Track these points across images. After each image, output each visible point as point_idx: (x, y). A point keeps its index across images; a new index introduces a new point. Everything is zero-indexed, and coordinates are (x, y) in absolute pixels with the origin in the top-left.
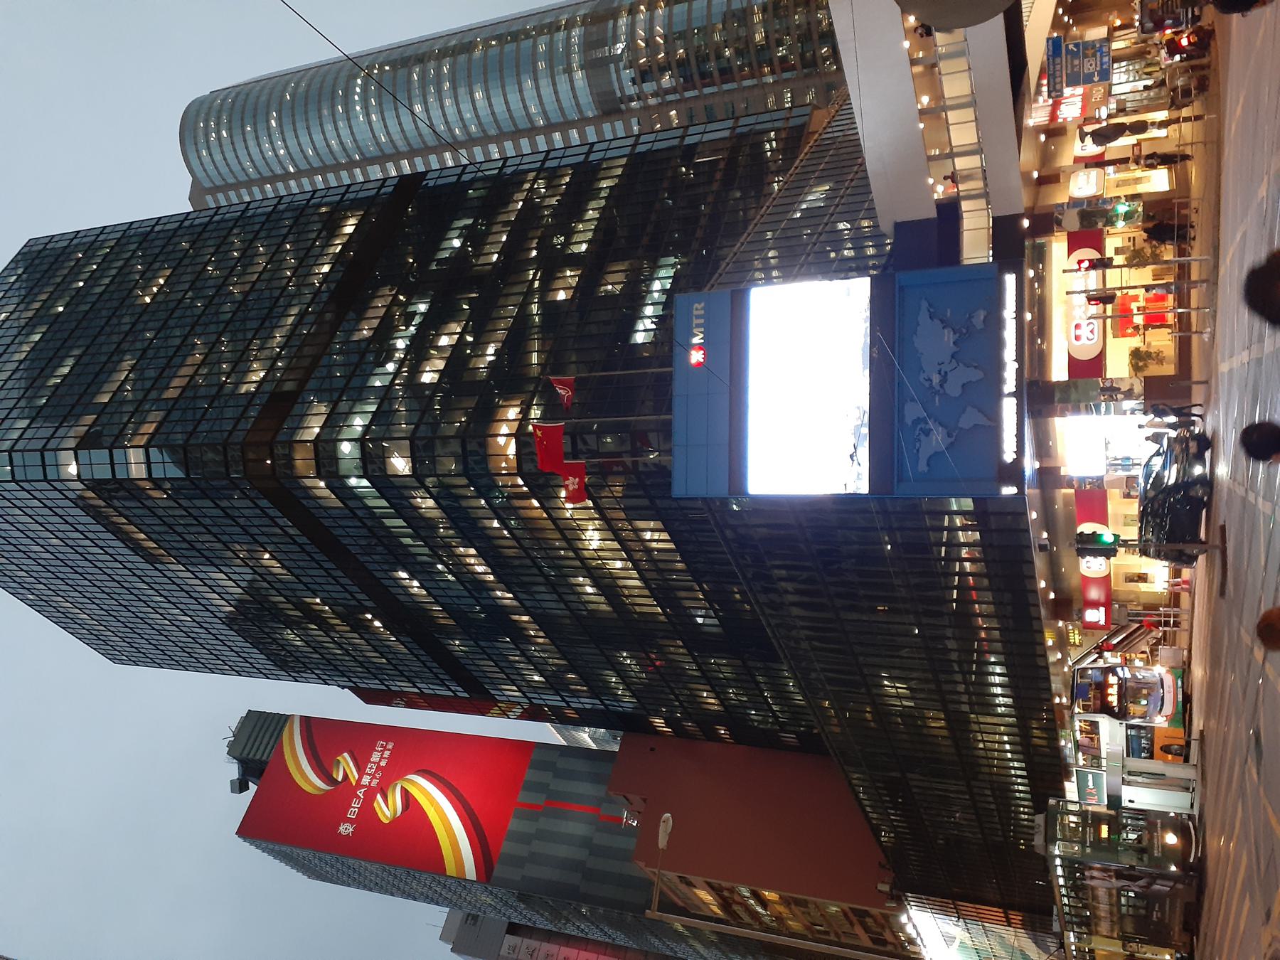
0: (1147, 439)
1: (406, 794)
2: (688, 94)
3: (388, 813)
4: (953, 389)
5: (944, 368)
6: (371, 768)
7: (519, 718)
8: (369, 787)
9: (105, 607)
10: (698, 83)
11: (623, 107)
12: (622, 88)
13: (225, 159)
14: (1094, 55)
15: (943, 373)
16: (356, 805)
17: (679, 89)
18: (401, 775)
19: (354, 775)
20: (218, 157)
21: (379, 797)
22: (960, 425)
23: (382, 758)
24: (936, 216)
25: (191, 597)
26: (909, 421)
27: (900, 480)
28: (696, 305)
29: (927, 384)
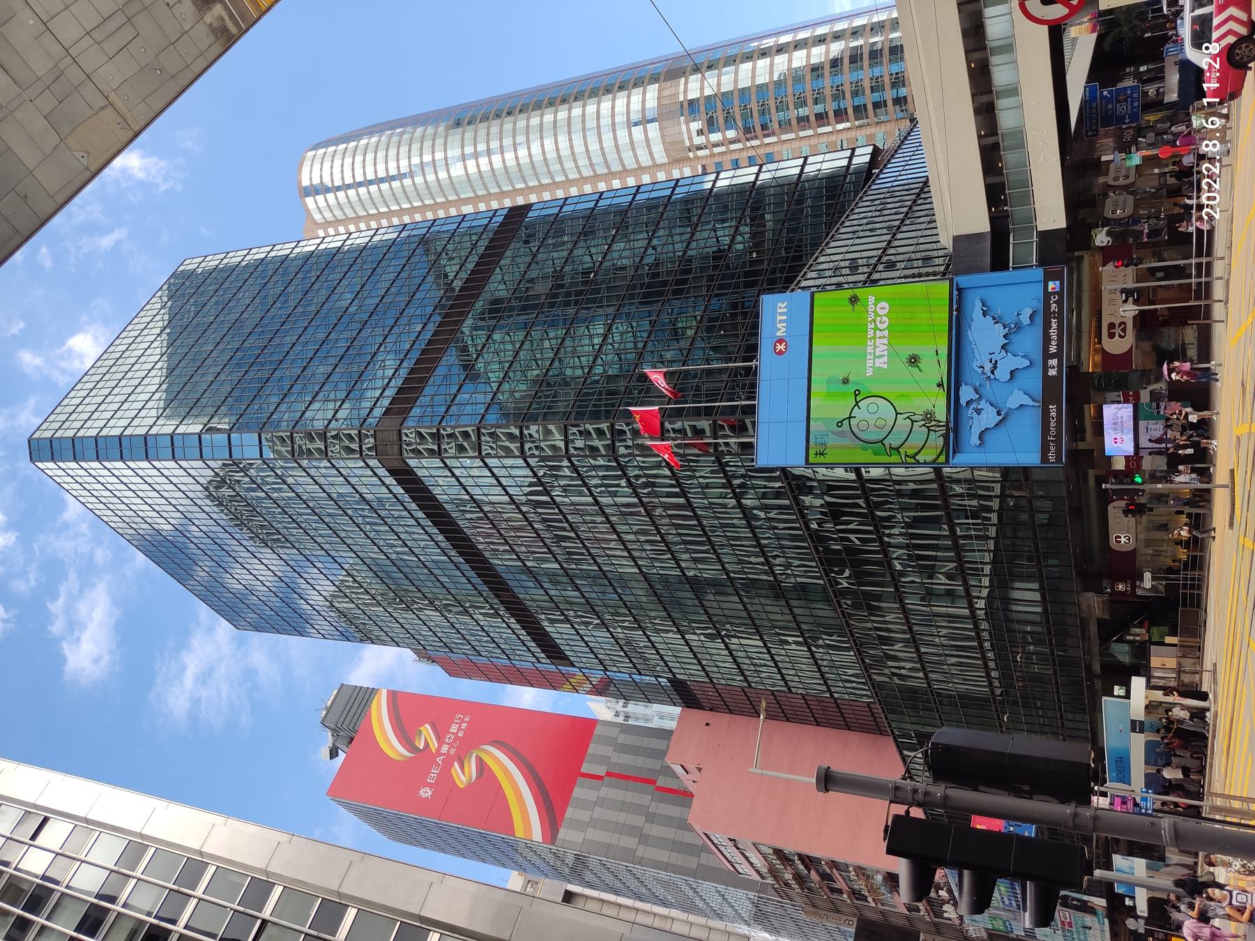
1: (480, 762)
4: (1003, 374)
5: (994, 358)
6: (449, 738)
7: (589, 693)
8: (447, 754)
11: (691, 155)
12: (690, 138)
16: (435, 771)
18: (477, 747)
19: (434, 744)
20: (594, 146)
21: (456, 764)
23: (459, 729)
24: (989, 230)
26: (963, 402)
28: (780, 304)
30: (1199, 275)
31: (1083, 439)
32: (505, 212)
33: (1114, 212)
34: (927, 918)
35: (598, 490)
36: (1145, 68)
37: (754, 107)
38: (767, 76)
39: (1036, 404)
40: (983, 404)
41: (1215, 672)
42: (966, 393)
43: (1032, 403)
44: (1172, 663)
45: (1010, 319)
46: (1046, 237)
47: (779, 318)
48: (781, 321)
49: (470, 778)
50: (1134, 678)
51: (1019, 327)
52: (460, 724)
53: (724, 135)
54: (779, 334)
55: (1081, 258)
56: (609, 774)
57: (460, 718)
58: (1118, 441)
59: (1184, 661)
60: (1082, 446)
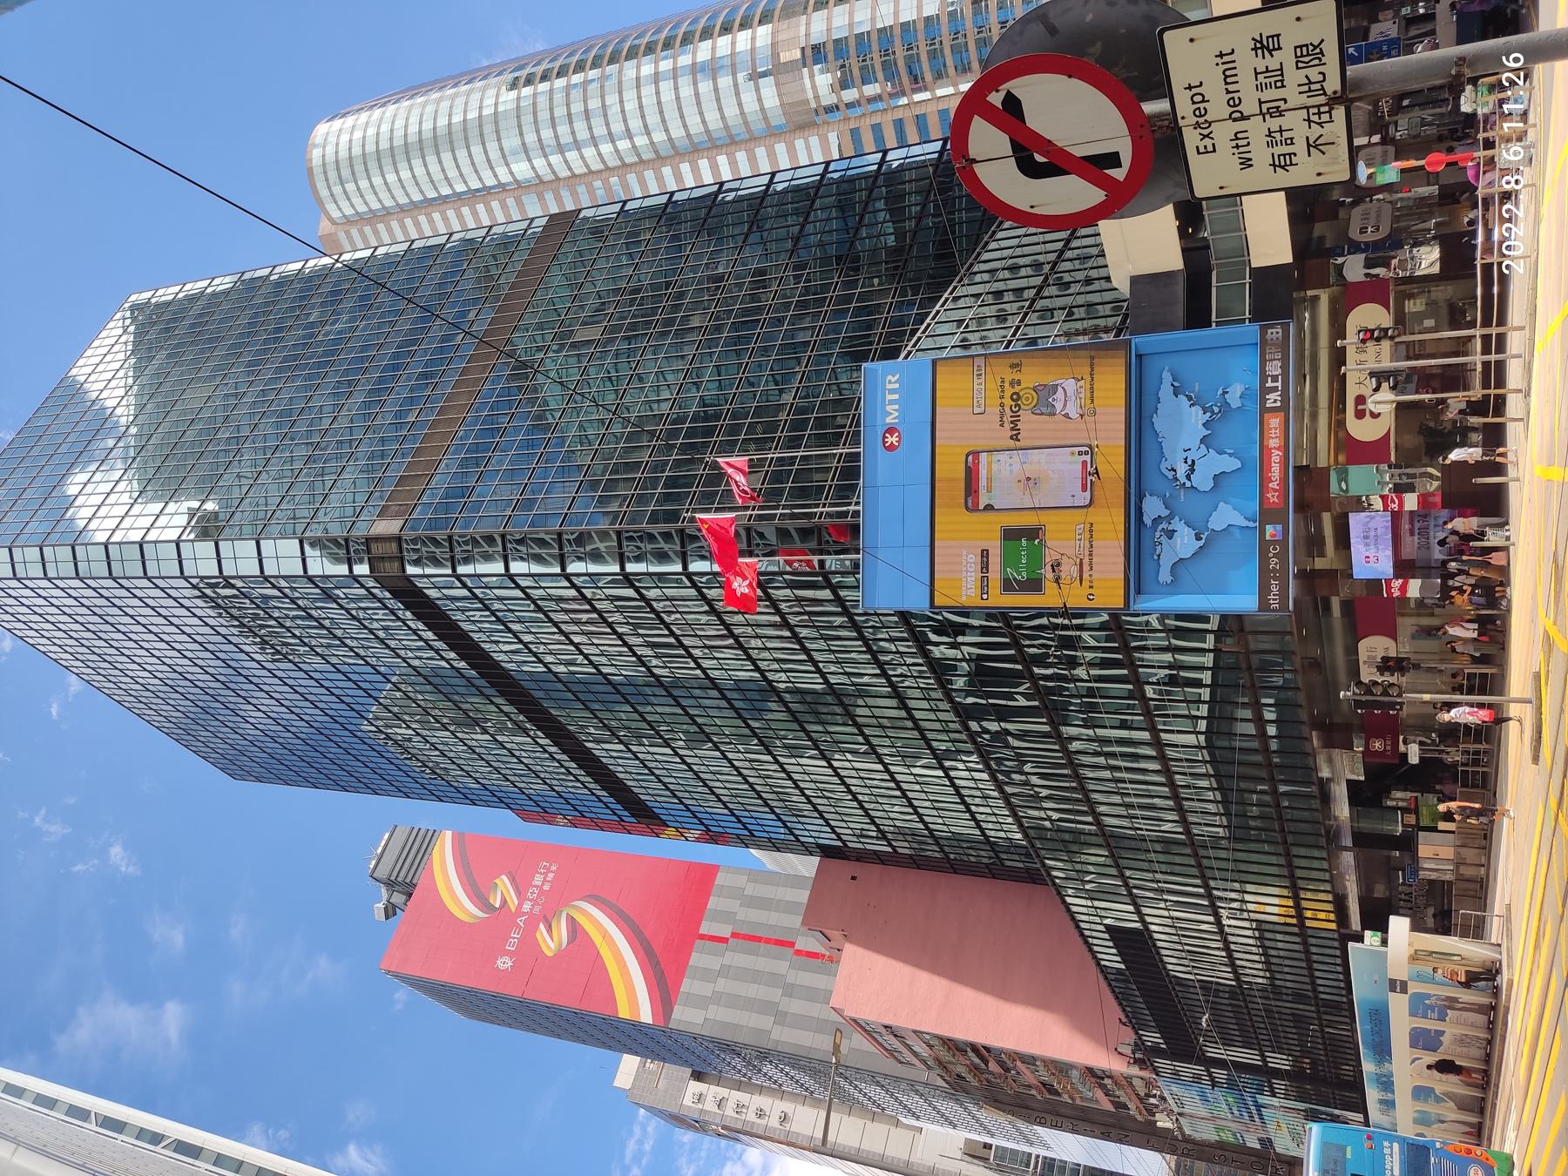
0: (1429, 1067)
1: (572, 922)
3: (552, 945)
4: (1202, 480)
6: (532, 893)
7: (698, 840)
8: (530, 914)
9: (221, 735)
10: (908, 90)
13: (428, 174)
15: (1190, 462)
16: (515, 936)
17: (885, 96)
19: (513, 901)
22: (1211, 526)
23: (545, 881)
25: (360, 688)
26: (1147, 520)
27: (1139, 592)
28: (890, 377)
29: (1170, 475)
30: (1486, 350)
31: (1322, 554)
32: (543, 221)
33: (1363, 230)
34: (1139, 1118)
35: (704, 580)
36: (1277, 760)
37: (900, 54)
38: (915, 10)
39: (1251, 524)
41: (1509, 919)
42: (1153, 507)
44: (1448, 852)
46: (1265, 276)
47: (889, 397)
48: (892, 402)
49: (561, 944)
50: (1392, 918)
52: (546, 874)
53: (861, 92)
54: (889, 420)
55: (1316, 298)
56: (734, 935)
58: (1371, 559)
59: (1464, 851)
60: (1320, 564)
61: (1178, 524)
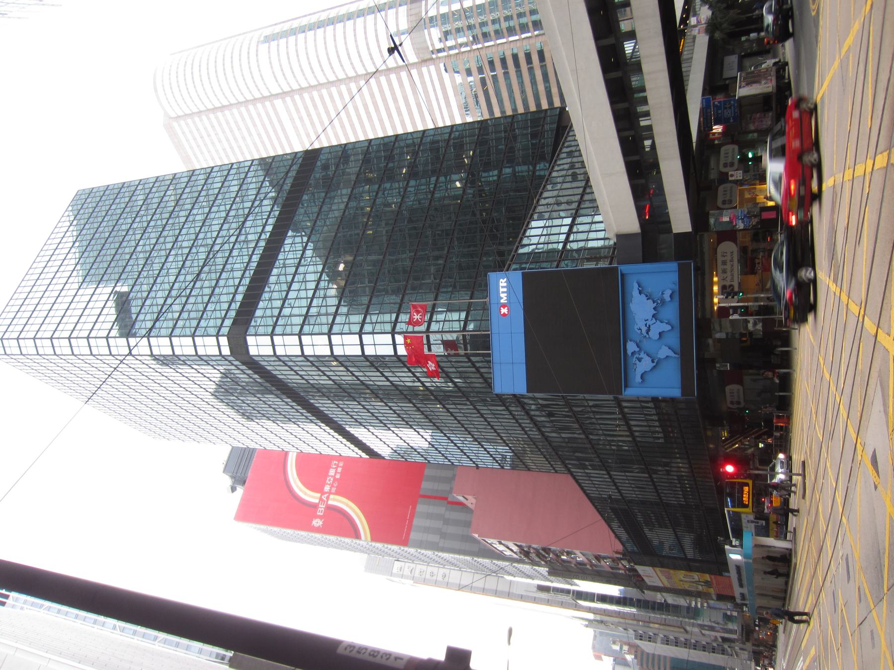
2: (475, 47)
4: (654, 334)
5: (649, 323)
11: (434, 56)
12: (433, 45)
14: (730, 108)
24: (639, 231)
26: (629, 352)
27: (626, 386)
28: (501, 280)
39: (677, 356)
40: (642, 355)
43: (675, 355)
45: (657, 295)
48: (503, 292)
51: (663, 302)
52: (336, 469)
57: (335, 464)
61: (642, 355)
